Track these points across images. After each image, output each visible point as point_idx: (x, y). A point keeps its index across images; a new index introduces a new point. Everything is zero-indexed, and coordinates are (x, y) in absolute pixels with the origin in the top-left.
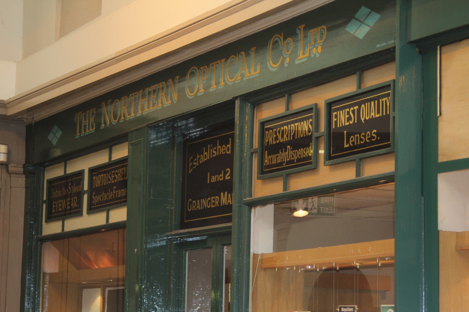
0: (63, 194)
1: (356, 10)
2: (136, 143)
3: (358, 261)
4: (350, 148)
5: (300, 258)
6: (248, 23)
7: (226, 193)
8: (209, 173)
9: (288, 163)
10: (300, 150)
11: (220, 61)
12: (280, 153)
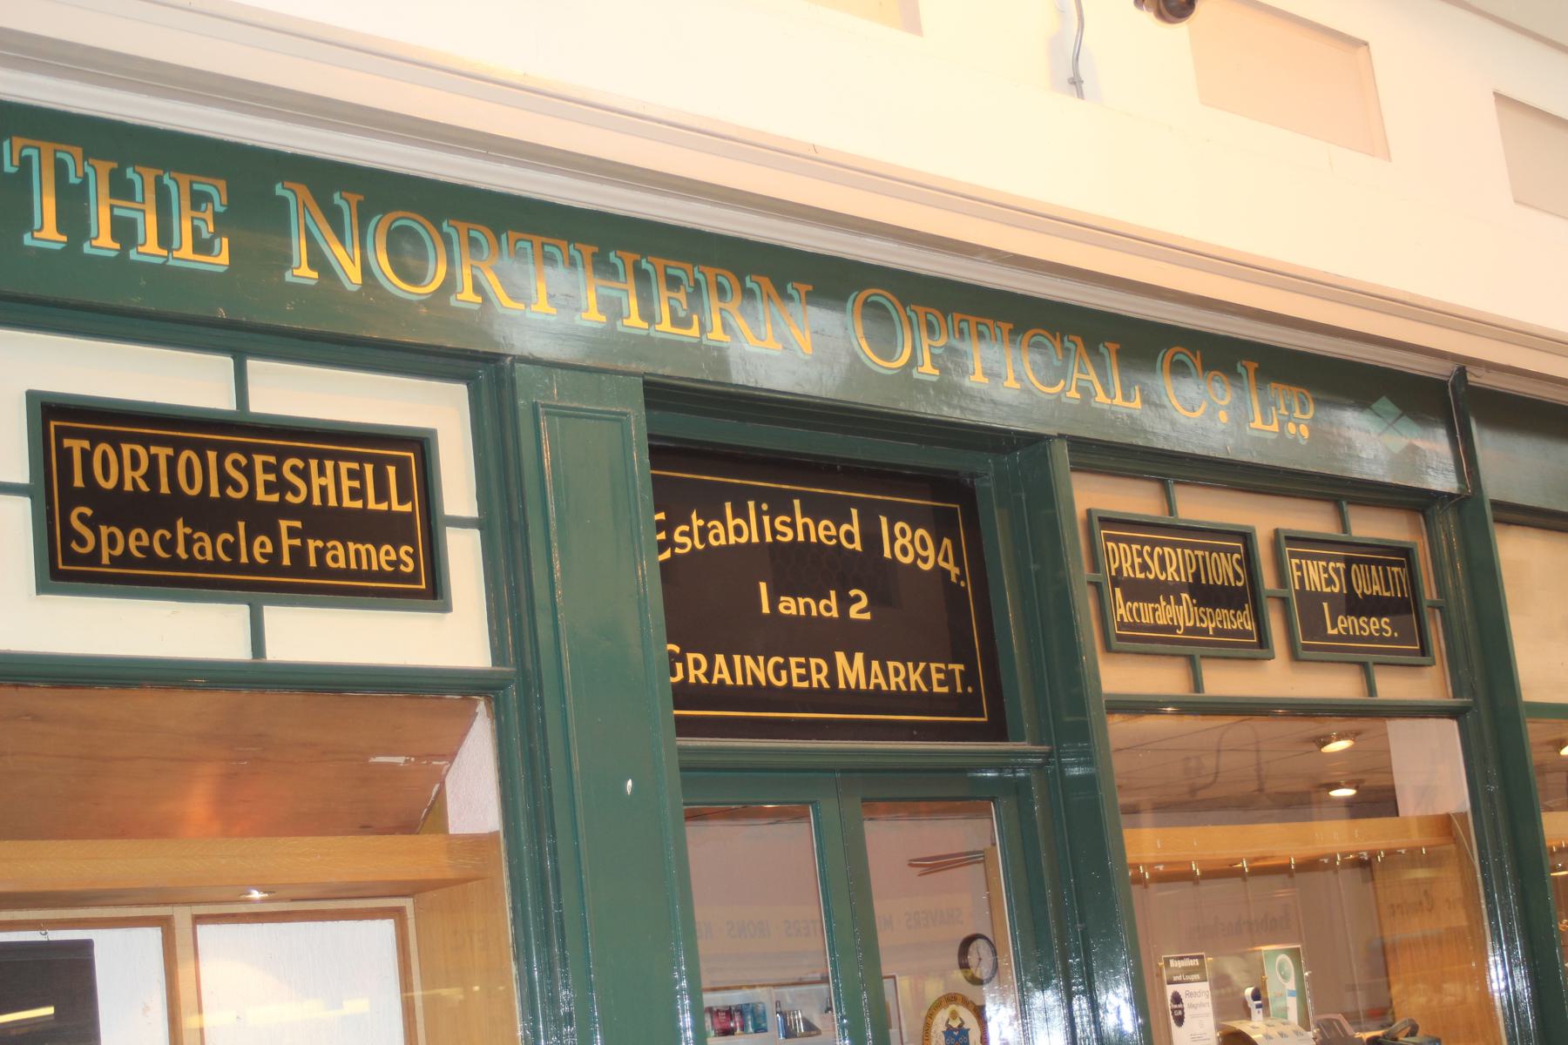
0: (1125, 558)
1: (1375, 399)
2: (582, 413)
3: (1200, 863)
4: (1339, 638)
5: (1195, 844)
6: (1232, 309)
7: (859, 657)
8: (763, 586)
9: (1188, 631)
10: (1218, 610)
11: (283, 184)
12: (1163, 603)
